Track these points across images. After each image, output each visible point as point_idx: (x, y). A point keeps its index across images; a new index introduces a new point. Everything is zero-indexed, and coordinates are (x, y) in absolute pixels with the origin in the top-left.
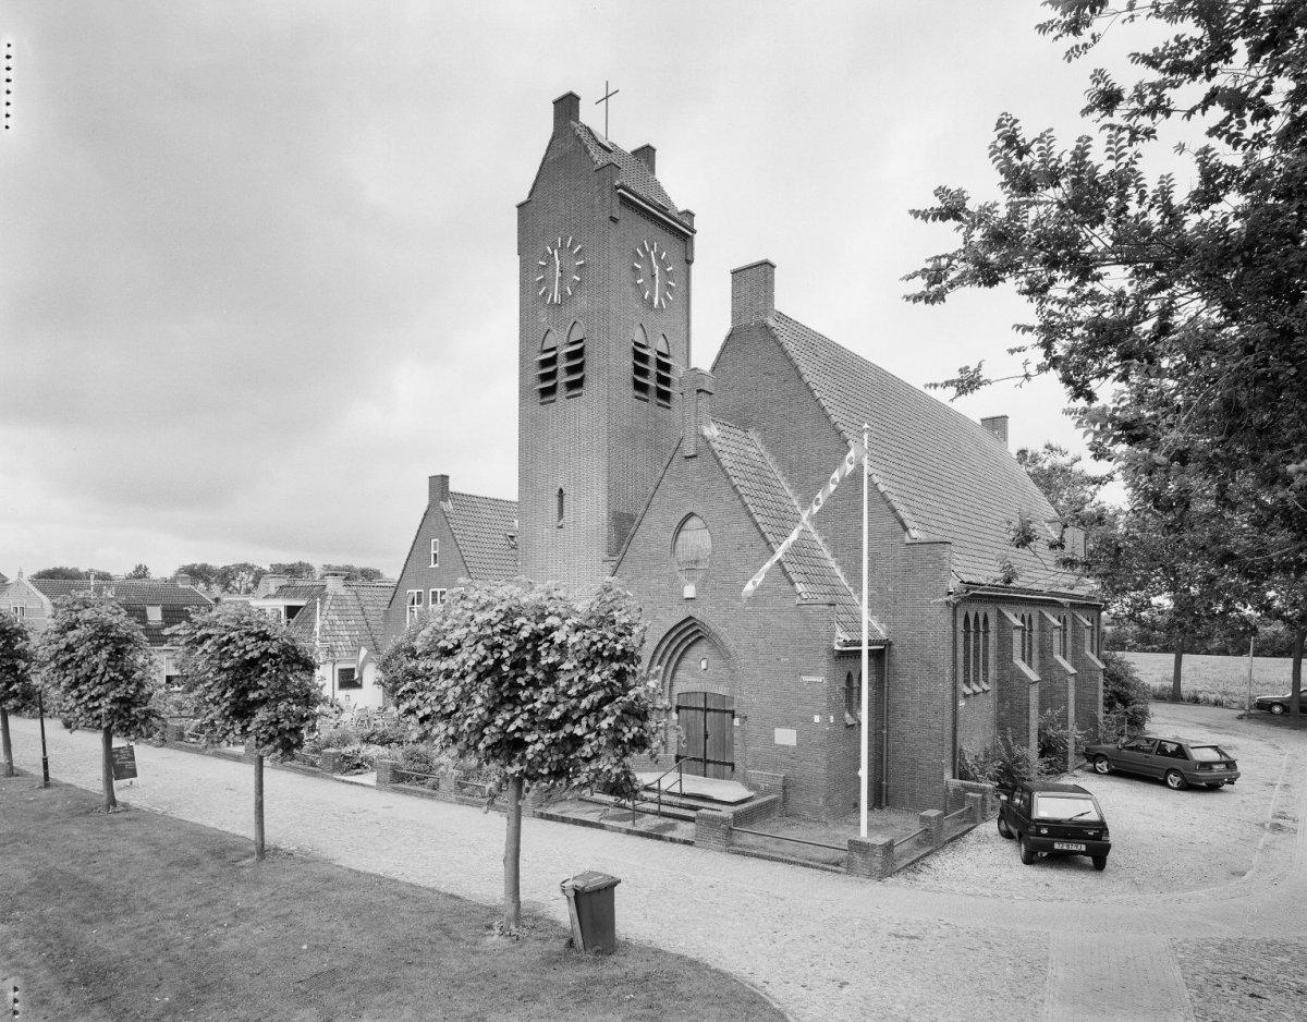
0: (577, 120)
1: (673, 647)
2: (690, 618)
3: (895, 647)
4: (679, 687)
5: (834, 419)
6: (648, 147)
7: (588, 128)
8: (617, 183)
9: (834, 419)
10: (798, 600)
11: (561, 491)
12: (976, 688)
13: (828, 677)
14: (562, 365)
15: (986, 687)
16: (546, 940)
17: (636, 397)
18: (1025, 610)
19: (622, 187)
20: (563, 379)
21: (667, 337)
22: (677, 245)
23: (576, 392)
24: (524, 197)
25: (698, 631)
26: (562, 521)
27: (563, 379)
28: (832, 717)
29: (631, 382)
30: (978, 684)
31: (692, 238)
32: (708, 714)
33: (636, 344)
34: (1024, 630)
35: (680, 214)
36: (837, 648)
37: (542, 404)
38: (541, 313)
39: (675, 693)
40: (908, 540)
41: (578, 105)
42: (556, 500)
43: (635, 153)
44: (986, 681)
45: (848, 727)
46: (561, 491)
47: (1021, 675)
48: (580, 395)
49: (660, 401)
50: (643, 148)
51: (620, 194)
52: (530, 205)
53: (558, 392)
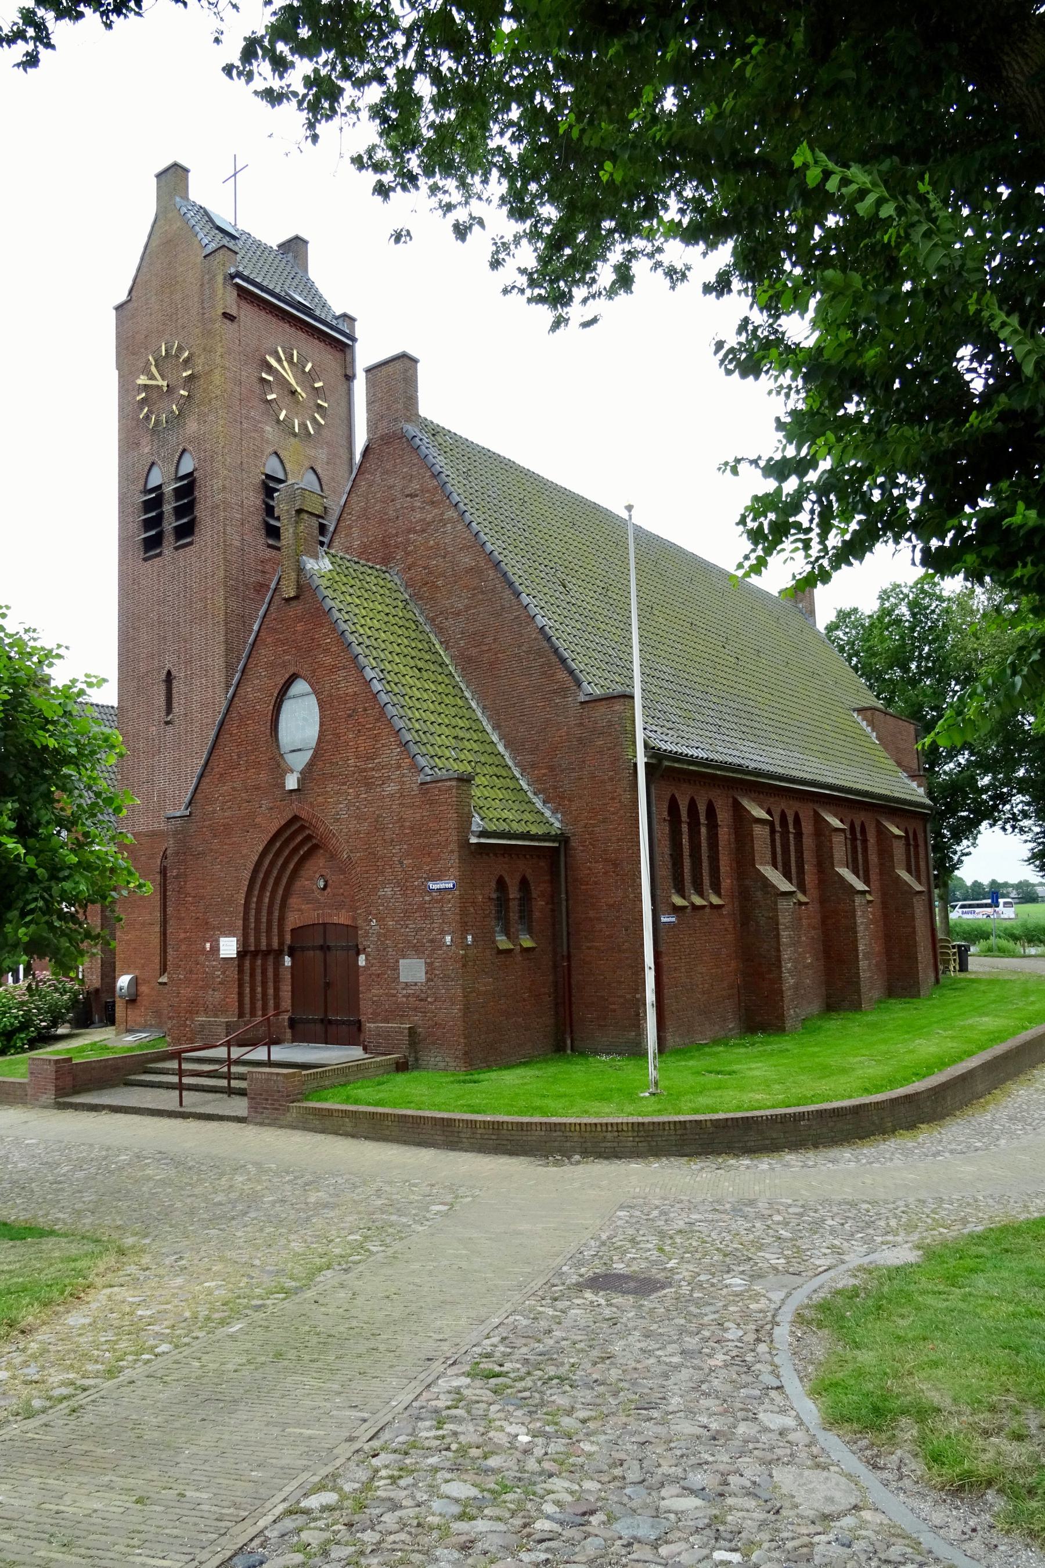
0: (186, 197)
1: (280, 862)
2: (295, 818)
3: (574, 843)
4: (293, 920)
5: (489, 547)
6: (297, 238)
7: (206, 213)
8: (232, 270)
9: (489, 547)
10: (421, 779)
11: (169, 673)
12: (698, 901)
13: (461, 880)
14: (168, 508)
15: (715, 900)
16: (443, 1437)
17: (270, 546)
18: (781, 805)
19: (238, 275)
20: (170, 524)
21: (319, 471)
22: (328, 357)
23: (188, 540)
24: (123, 297)
25: (309, 838)
26: (170, 717)
27: (170, 524)
28: (470, 938)
29: (262, 526)
30: (701, 894)
31: (351, 348)
32: (321, 942)
33: (268, 476)
34: (771, 824)
35: (337, 318)
36: (473, 840)
37: (145, 560)
38: (144, 441)
39: (288, 928)
40: (582, 698)
41: (187, 179)
42: (163, 687)
43: (280, 246)
44: (718, 893)
45: (500, 952)
46: (169, 673)
47: (766, 883)
48: (191, 543)
49: (270, 542)
50: (290, 241)
51: (238, 285)
52: (130, 305)
53: (165, 543)
